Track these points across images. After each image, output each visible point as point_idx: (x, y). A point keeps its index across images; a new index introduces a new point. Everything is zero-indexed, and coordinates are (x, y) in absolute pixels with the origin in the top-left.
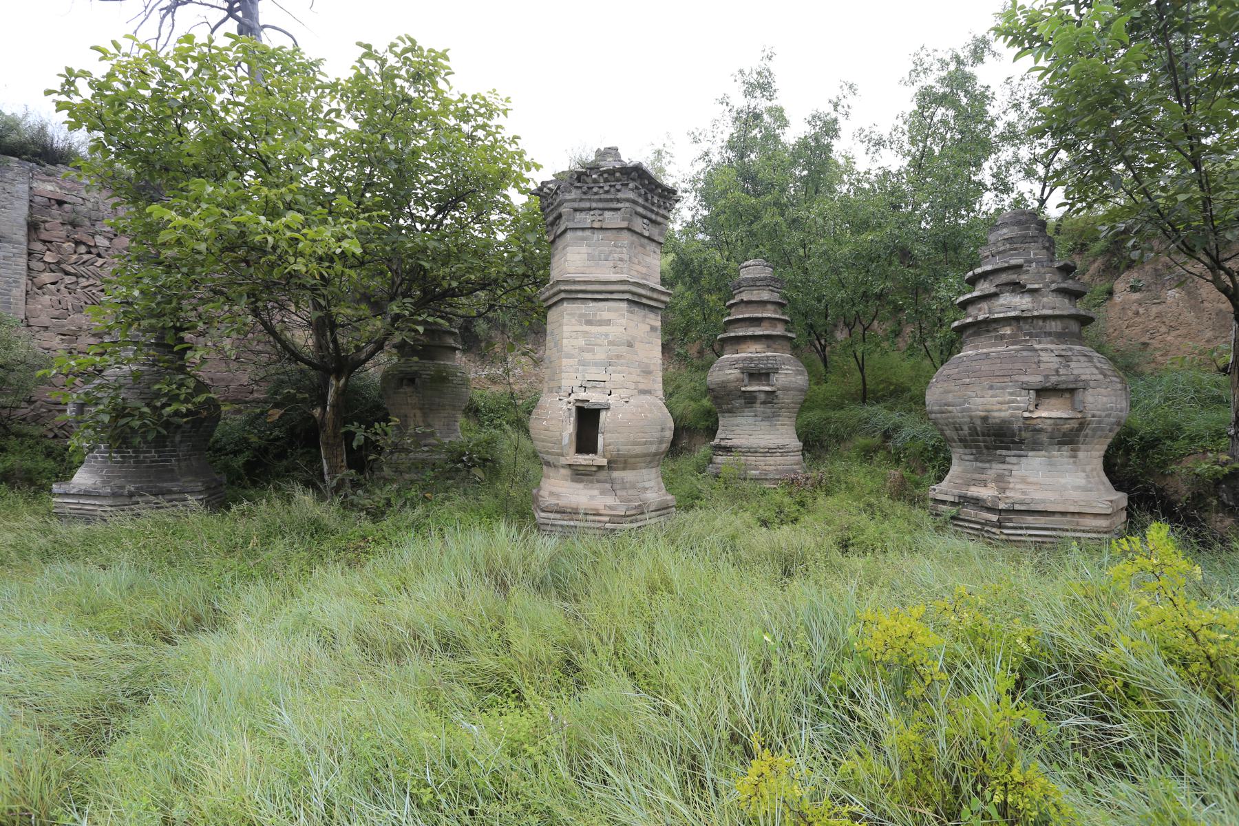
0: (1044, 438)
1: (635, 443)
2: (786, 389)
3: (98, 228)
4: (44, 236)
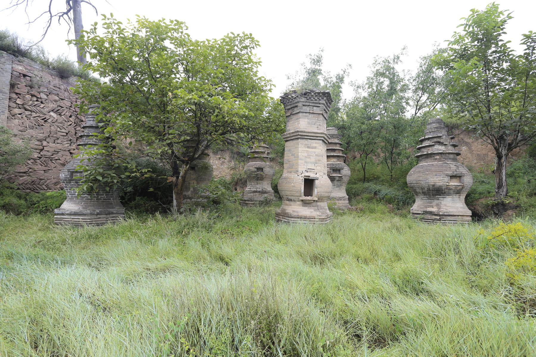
0: (452, 192)
1: (326, 192)
2: (345, 176)
3: (41, 89)
4: (17, 91)
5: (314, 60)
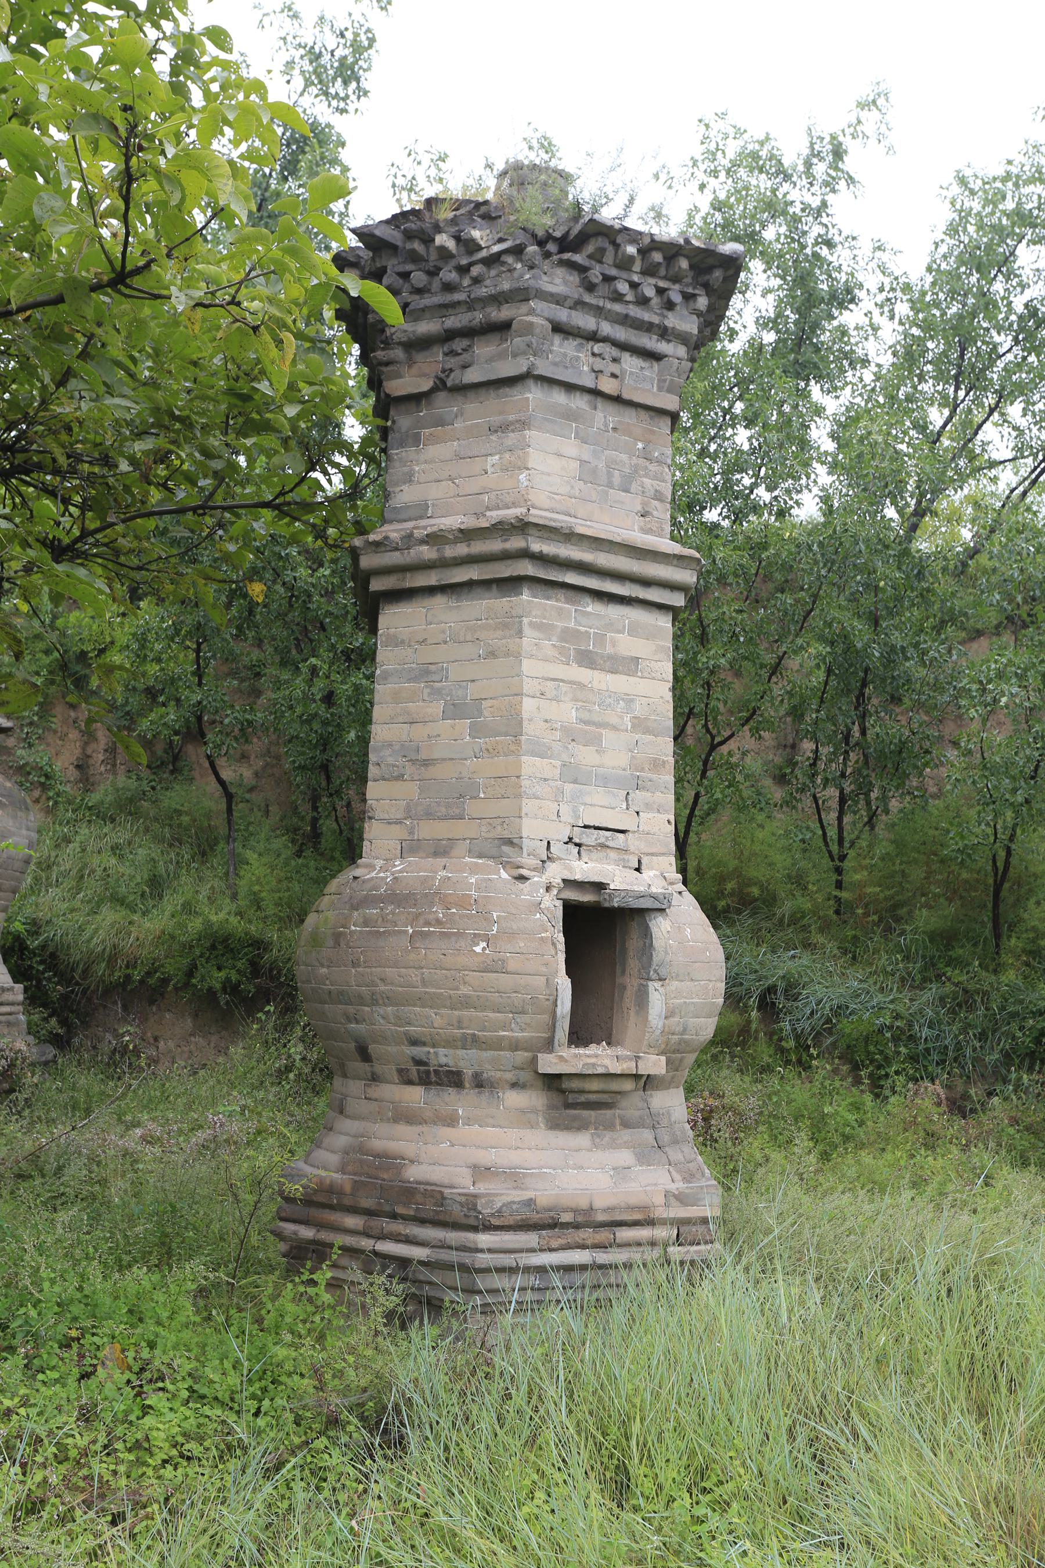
5: (315, 56)
